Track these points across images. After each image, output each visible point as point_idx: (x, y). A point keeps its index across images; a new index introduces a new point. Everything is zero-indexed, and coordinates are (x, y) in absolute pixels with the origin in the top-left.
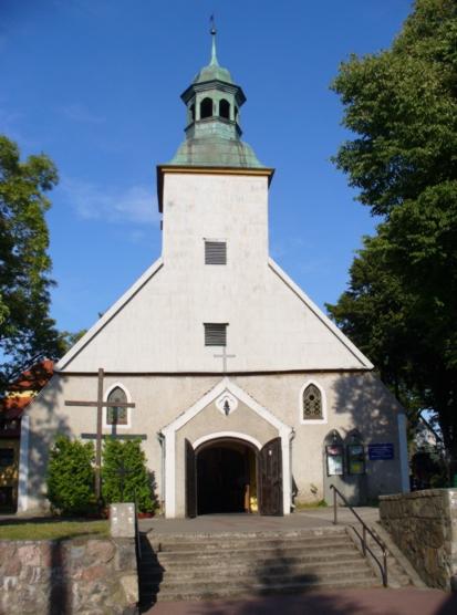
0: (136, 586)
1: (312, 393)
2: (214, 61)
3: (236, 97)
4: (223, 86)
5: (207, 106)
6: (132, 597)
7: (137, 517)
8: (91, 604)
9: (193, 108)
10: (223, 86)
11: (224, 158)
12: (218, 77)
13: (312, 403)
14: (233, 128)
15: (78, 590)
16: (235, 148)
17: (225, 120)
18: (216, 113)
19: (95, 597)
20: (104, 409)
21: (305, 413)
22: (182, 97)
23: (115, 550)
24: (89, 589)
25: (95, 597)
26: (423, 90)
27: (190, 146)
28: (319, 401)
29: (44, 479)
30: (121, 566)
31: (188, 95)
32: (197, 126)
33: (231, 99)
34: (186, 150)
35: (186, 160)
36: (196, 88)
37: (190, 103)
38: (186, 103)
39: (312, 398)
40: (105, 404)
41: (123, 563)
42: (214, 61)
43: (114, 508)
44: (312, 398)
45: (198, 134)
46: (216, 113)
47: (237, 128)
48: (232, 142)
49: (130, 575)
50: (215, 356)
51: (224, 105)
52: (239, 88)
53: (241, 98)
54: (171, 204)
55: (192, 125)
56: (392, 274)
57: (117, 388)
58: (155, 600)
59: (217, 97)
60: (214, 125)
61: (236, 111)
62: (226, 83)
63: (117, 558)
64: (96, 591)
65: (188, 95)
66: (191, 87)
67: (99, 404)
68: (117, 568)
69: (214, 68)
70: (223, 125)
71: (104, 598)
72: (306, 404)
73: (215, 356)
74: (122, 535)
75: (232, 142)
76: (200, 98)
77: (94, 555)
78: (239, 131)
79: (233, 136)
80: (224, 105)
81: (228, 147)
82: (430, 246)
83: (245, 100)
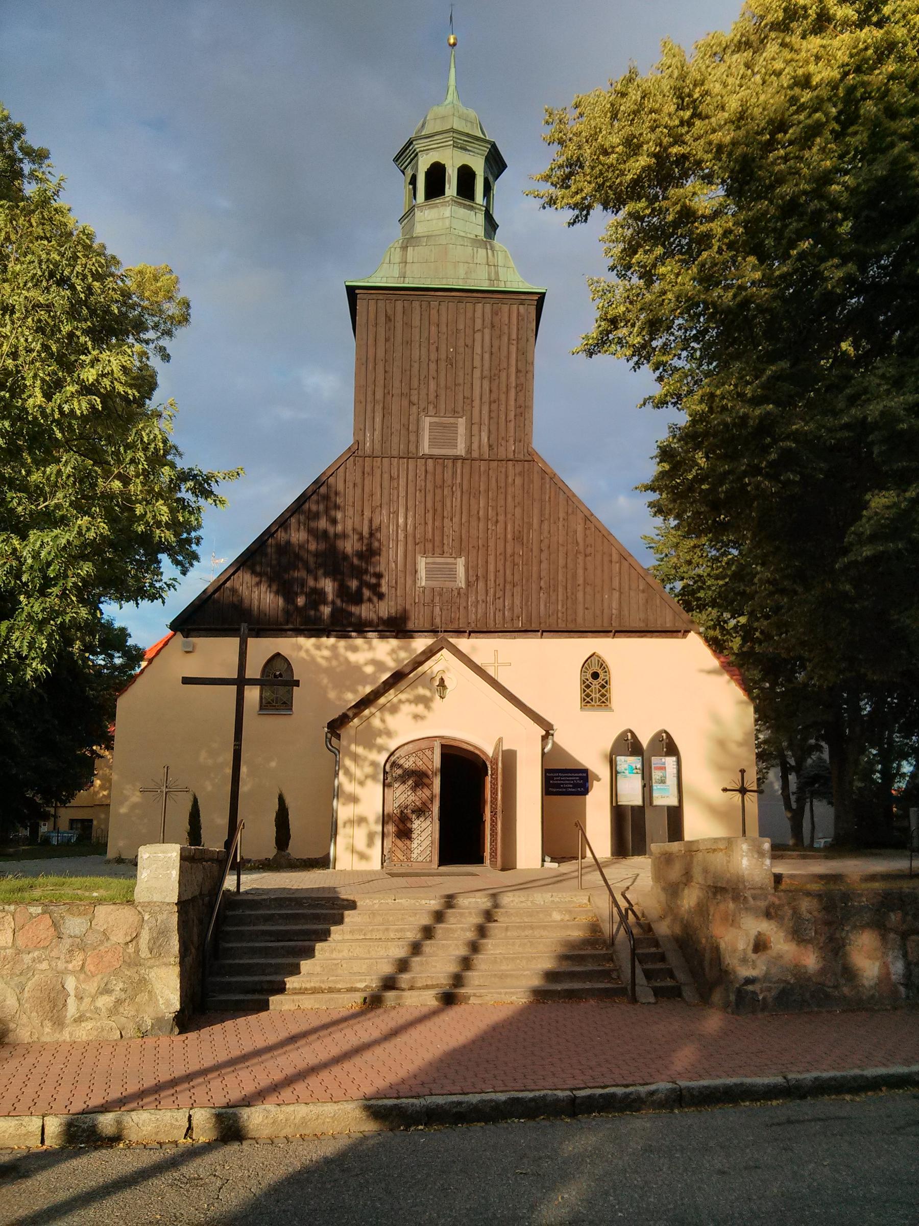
0: (175, 983)
1: (596, 668)
2: (451, 96)
4: (463, 141)
5: (436, 175)
6: (168, 1003)
7: (909, 826)
8: (97, 1010)
9: (413, 181)
10: (463, 141)
12: (458, 125)
13: (596, 684)
14: (481, 218)
15: (77, 988)
16: (482, 252)
18: (451, 188)
19: (104, 1002)
22: (396, 160)
24: (92, 987)
25: (104, 1002)
31: (405, 156)
32: (418, 214)
33: (478, 166)
34: (397, 256)
36: (418, 146)
37: (409, 172)
39: (595, 676)
41: (156, 947)
42: (451, 96)
43: (145, 853)
44: (595, 676)
45: (419, 229)
46: (451, 188)
47: (489, 217)
49: (167, 965)
51: (466, 176)
52: (494, 146)
55: (412, 210)
58: (264, 1006)
59: (452, 161)
60: (447, 211)
62: (468, 135)
63: (145, 936)
64: (106, 991)
65: (405, 156)
66: (410, 143)
67: (241, 682)
68: (144, 953)
69: (451, 109)
71: (119, 1002)
75: (475, 242)
76: (424, 164)
78: (491, 225)
79: (480, 232)
81: (469, 250)
82: (12, 148)
83: (504, 166)
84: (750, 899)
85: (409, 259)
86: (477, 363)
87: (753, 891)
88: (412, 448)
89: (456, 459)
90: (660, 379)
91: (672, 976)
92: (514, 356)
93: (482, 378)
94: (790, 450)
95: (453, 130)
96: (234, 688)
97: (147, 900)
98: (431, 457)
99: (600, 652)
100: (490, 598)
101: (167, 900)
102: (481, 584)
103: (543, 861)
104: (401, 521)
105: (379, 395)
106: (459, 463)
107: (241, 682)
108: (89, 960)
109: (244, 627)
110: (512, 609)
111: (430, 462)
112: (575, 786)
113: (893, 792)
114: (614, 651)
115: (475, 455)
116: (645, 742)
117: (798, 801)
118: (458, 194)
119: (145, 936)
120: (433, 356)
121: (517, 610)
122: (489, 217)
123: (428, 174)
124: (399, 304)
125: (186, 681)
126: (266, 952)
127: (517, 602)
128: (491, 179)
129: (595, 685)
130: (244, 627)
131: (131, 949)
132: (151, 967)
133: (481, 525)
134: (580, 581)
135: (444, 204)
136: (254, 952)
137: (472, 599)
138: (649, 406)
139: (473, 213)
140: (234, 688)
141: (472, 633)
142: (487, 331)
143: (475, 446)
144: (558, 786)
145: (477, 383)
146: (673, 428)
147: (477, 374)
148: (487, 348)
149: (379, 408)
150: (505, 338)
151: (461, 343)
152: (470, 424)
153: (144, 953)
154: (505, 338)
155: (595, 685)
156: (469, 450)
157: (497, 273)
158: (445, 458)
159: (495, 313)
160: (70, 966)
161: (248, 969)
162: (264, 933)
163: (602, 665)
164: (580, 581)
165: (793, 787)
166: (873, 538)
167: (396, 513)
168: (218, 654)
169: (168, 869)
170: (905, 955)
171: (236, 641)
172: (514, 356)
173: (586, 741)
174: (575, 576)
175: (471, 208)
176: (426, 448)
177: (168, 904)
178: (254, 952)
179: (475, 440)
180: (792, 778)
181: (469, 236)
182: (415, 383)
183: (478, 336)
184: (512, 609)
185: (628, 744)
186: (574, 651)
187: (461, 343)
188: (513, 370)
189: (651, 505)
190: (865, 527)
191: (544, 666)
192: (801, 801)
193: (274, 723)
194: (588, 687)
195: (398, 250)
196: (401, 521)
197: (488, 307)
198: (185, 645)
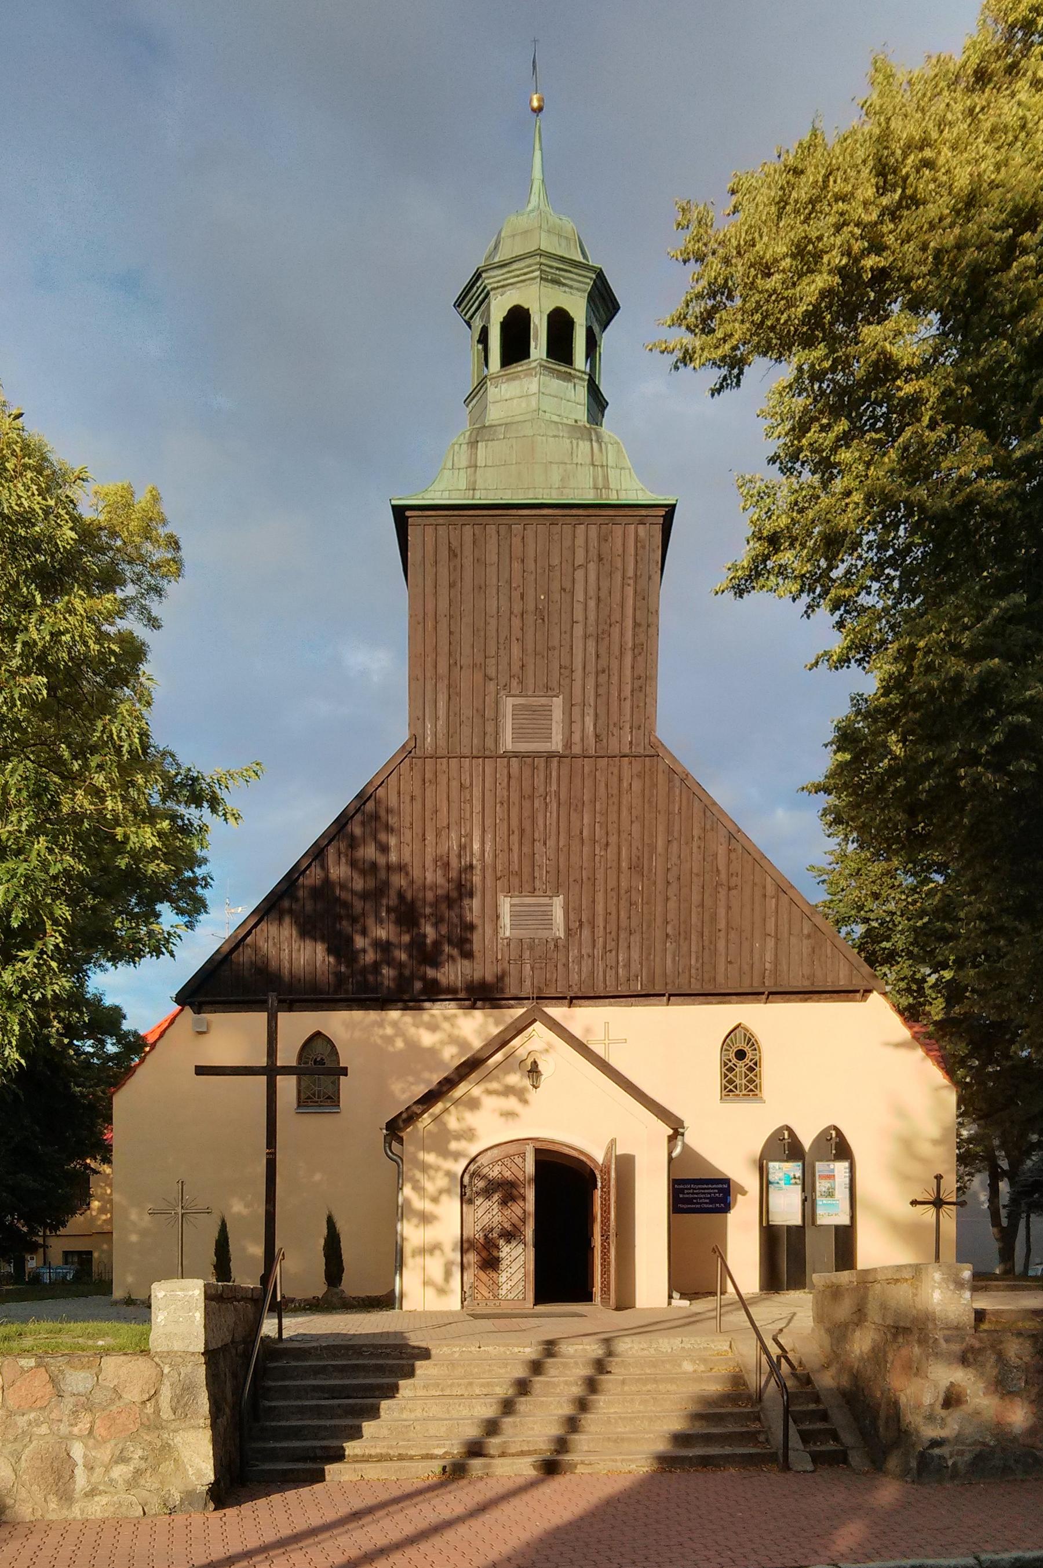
3: (591, 298)
4: (555, 269)
6: (199, 1474)
9: (484, 338)
10: (555, 269)
11: (555, 476)
12: (548, 244)
13: (741, 1067)
14: (582, 393)
15: (85, 1456)
16: (584, 446)
17: (539, 1145)
18: (539, 347)
19: (120, 1472)
22: (458, 304)
24: (104, 1454)
25: (120, 1472)
27: (473, 444)
29: (94, 1213)
31: (472, 297)
32: (493, 391)
33: (578, 309)
35: (463, 485)
36: (490, 280)
37: (478, 323)
39: (741, 1055)
40: (287, 1071)
41: (181, 1405)
42: (536, 198)
45: (494, 414)
46: (539, 347)
50: (939, 1178)
51: (560, 324)
52: (600, 275)
53: (604, 303)
54: (812, 977)
55: (482, 383)
57: (318, 1034)
59: (540, 302)
60: (533, 385)
62: (562, 259)
64: (122, 1459)
65: (472, 297)
66: (478, 276)
67: (271, 1071)
68: (166, 1414)
71: (138, 1473)
72: (728, 1069)
73: (939, 1178)
75: (575, 430)
76: (498, 309)
77: (115, 1390)
78: (597, 402)
79: (581, 414)
80: (560, 324)
84: (942, 1341)
85: (480, 462)
86: (579, 615)
87: (946, 1332)
88: (490, 743)
89: (550, 756)
91: (836, 1438)
93: (586, 637)
95: (541, 253)
98: (516, 755)
99: (746, 1023)
100: (598, 951)
102: (586, 932)
103: (670, 1297)
105: (443, 668)
109: (272, 998)
110: (628, 965)
112: (713, 1200)
114: (766, 1020)
115: (577, 750)
116: (807, 1141)
118: (549, 355)
120: (517, 608)
121: (635, 967)
123: (505, 325)
128: (596, 329)
129: (741, 1067)
130: (272, 998)
131: (149, 1409)
132: (175, 1431)
135: (528, 373)
137: (573, 953)
139: (571, 385)
141: (572, 1000)
142: (592, 566)
143: (576, 737)
144: (689, 1201)
146: (857, 700)
148: (592, 592)
149: (442, 686)
151: (556, 586)
153: (166, 1414)
155: (741, 1067)
156: (568, 744)
157: (606, 478)
158: (537, 755)
159: (603, 539)
160: (76, 1430)
161: (296, 1433)
162: (315, 1388)
163: (751, 1040)
171: (260, 1018)
174: (714, 918)
176: (508, 743)
179: (577, 728)
181: (565, 421)
182: (492, 650)
183: (579, 574)
184: (628, 965)
185: (785, 1145)
187: (556, 586)
188: (629, 623)
191: (671, 1042)
193: (316, 1124)
194: (731, 1070)
195: (464, 447)
198: (196, 1023)
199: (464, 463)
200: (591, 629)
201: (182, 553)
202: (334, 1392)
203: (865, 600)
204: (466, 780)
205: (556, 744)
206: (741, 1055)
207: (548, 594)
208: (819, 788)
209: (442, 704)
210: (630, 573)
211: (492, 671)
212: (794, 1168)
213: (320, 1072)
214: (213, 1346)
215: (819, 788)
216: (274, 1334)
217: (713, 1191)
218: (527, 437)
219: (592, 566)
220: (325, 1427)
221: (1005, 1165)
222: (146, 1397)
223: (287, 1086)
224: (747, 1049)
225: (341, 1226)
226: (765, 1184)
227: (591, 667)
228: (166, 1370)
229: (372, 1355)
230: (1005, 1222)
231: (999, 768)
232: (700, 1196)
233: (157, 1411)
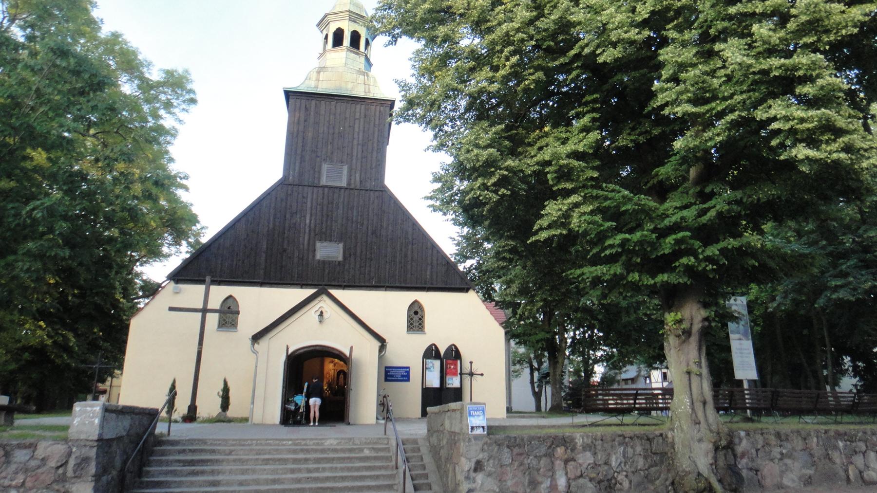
1: (416, 308)
9: (326, 37)
13: (416, 318)
14: (363, 59)
16: (362, 77)
17: (355, 50)
18: (347, 41)
20: (459, 371)
21: (408, 327)
22: (318, 25)
23: (70, 454)
26: (669, 471)
28: (423, 317)
30: (75, 472)
31: (322, 23)
37: (325, 32)
38: (322, 32)
44: (416, 313)
46: (347, 41)
48: (360, 72)
56: (607, 354)
57: (230, 297)
59: (348, 29)
61: (367, 43)
62: (357, 14)
63: (72, 462)
66: (326, 16)
67: (205, 311)
68: (70, 473)
70: (352, 55)
74: (83, 437)
76: (333, 28)
77: (43, 459)
79: (362, 67)
85: (321, 78)
86: (356, 135)
88: (316, 181)
89: (341, 188)
90: (436, 136)
92: (376, 134)
93: (358, 144)
94: (503, 175)
95: (350, 11)
96: (200, 314)
97: (76, 438)
98: (326, 187)
99: (419, 300)
100: (358, 266)
101: (91, 438)
102: (352, 259)
103: (377, 419)
104: (308, 221)
105: (299, 152)
106: (343, 191)
107: (205, 311)
108: (28, 479)
109: (208, 279)
110: (369, 274)
111: (326, 189)
112: (403, 376)
113: (129, 253)
114: (426, 298)
115: (352, 186)
116: (442, 351)
117: (538, 386)
119: (72, 462)
120: (331, 132)
121: (372, 274)
122: (367, 60)
124: (313, 102)
125: (171, 309)
126: (174, 473)
127: (373, 270)
128: (370, 40)
129: (416, 319)
130: (208, 279)
131: (61, 471)
132: (73, 483)
133: (354, 225)
134: (409, 258)
136: (167, 473)
137: (347, 267)
138: (430, 151)
140: (200, 314)
141: (344, 287)
142: (362, 120)
143: (352, 182)
144: (392, 376)
145: (355, 147)
146: (442, 163)
147: (355, 142)
148: (361, 128)
149: (298, 158)
150: (372, 124)
151: (347, 124)
152: (350, 170)
153: (70, 473)
154: (372, 124)
155: (416, 319)
156: (349, 184)
158: (336, 188)
159: (367, 110)
160: (14, 483)
162: (179, 461)
163: (421, 307)
164: (409, 258)
165: (536, 380)
166: (550, 227)
167: (305, 217)
168: (193, 294)
169: (93, 417)
170: (566, 474)
171: (201, 288)
172: (376, 134)
173: (407, 350)
174: (406, 256)
175: (357, 54)
176: (324, 181)
177: (92, 441)
178: (167, 473)
179: (353, 178)
180: (536, 374)
182: (320, 146)
183: (357, 122)
184: (369, 274)
185: (432, 352)
186: (406, 298)
187: (347, 124)
188: (376, 140)
189: (429, 206)
190: (544, 222)
191: (385, 307)
192: (540, 386)
193: (226, 336)
196: (308, 221)
197: (363, 107)
198: (175, 288)
199: (314, 78)
200: (360, 142)
201: (374, 71)
202: (192, 463)
203: (446, 128)
204: (305, 195)
205: (344, 184)
206: (416, 313)
207: (344, 127)
208: (427, 198)
209: (297, 164)
210: (377, 123)
211: (319, 154)
212: (437, 363)
213: (229, 314)
214: (107, 436)
215: (427, 198)
216: (165, 431)
217: (403, 372)
218: (339, 73)
219: (362, 120)
220: (175, 482)
221: (535, 365)
222: (59, 464)
223: (213, 319)
224: (419, 311)
225: (229, 384)
226: (424, 369)
227: (359, 156)
228: (74, 450)
229: (211, 444)
230: (537, 390)
231: (496, 192)
232: (392, 375)
233: (64, 473)
